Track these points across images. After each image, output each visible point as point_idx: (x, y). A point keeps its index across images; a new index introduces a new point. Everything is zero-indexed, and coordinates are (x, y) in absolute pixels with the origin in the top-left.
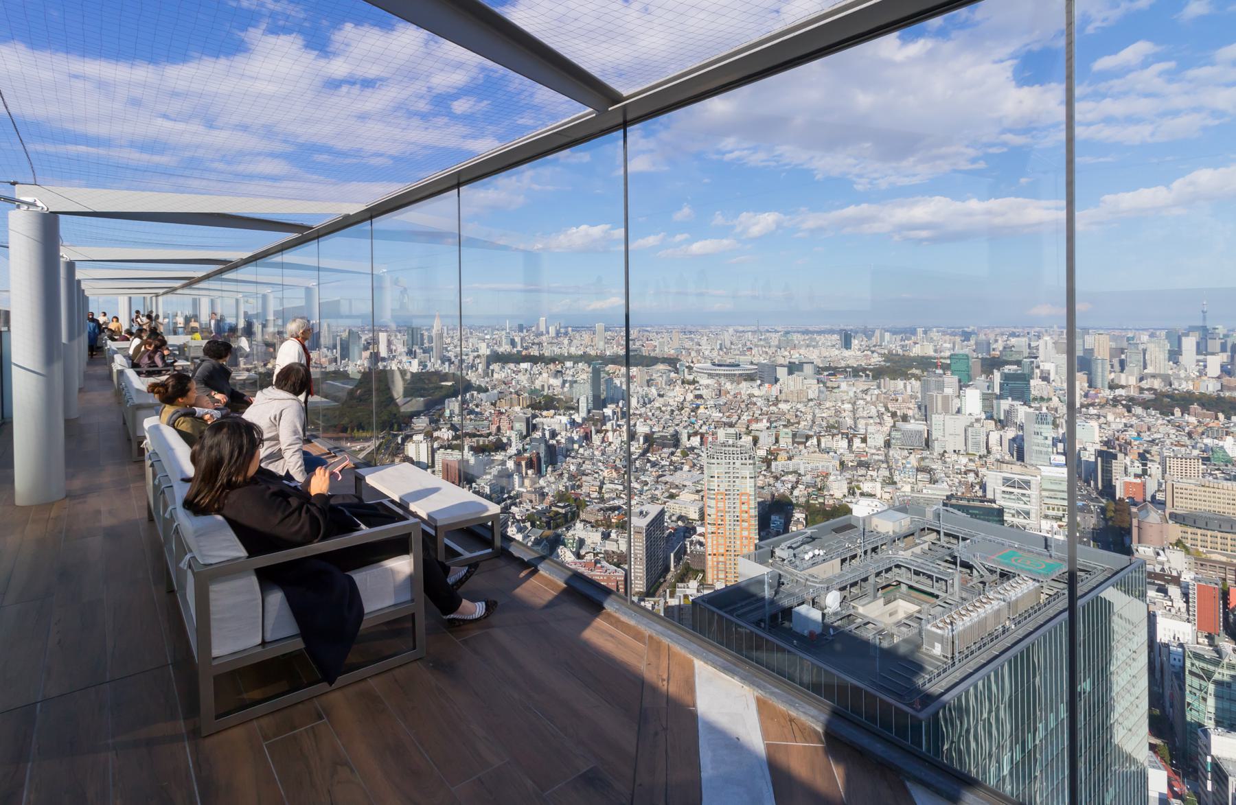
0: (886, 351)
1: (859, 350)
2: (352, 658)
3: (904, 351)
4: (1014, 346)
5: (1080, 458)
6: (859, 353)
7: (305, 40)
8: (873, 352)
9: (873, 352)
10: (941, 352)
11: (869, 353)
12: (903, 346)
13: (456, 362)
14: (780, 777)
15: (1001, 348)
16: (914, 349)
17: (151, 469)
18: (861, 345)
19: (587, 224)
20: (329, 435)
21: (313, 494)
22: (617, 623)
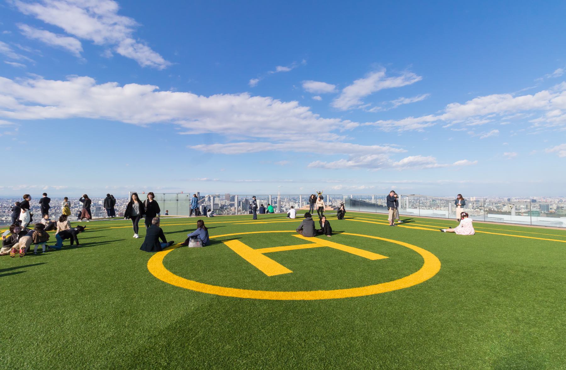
0: (488, 209)
1: (473, 208)
2: (193, 305)
3: (498, 209)
4: (563, 207)
5: (138, 238)
6: (472, 210)
7: (249, 95)
8: (480, 210)
9: (480, 210)
10: (519, 210)
11: (478, 210)
12: (497, 207)
13: (69, 330)
14: (44, 4)
15: (555, 208)
16: (504, 208)
17: (498, 204)
18: (473, 206)
19: (382, 120)
20: (5, 246)
21: (335, 106)
22: (195, 222)
